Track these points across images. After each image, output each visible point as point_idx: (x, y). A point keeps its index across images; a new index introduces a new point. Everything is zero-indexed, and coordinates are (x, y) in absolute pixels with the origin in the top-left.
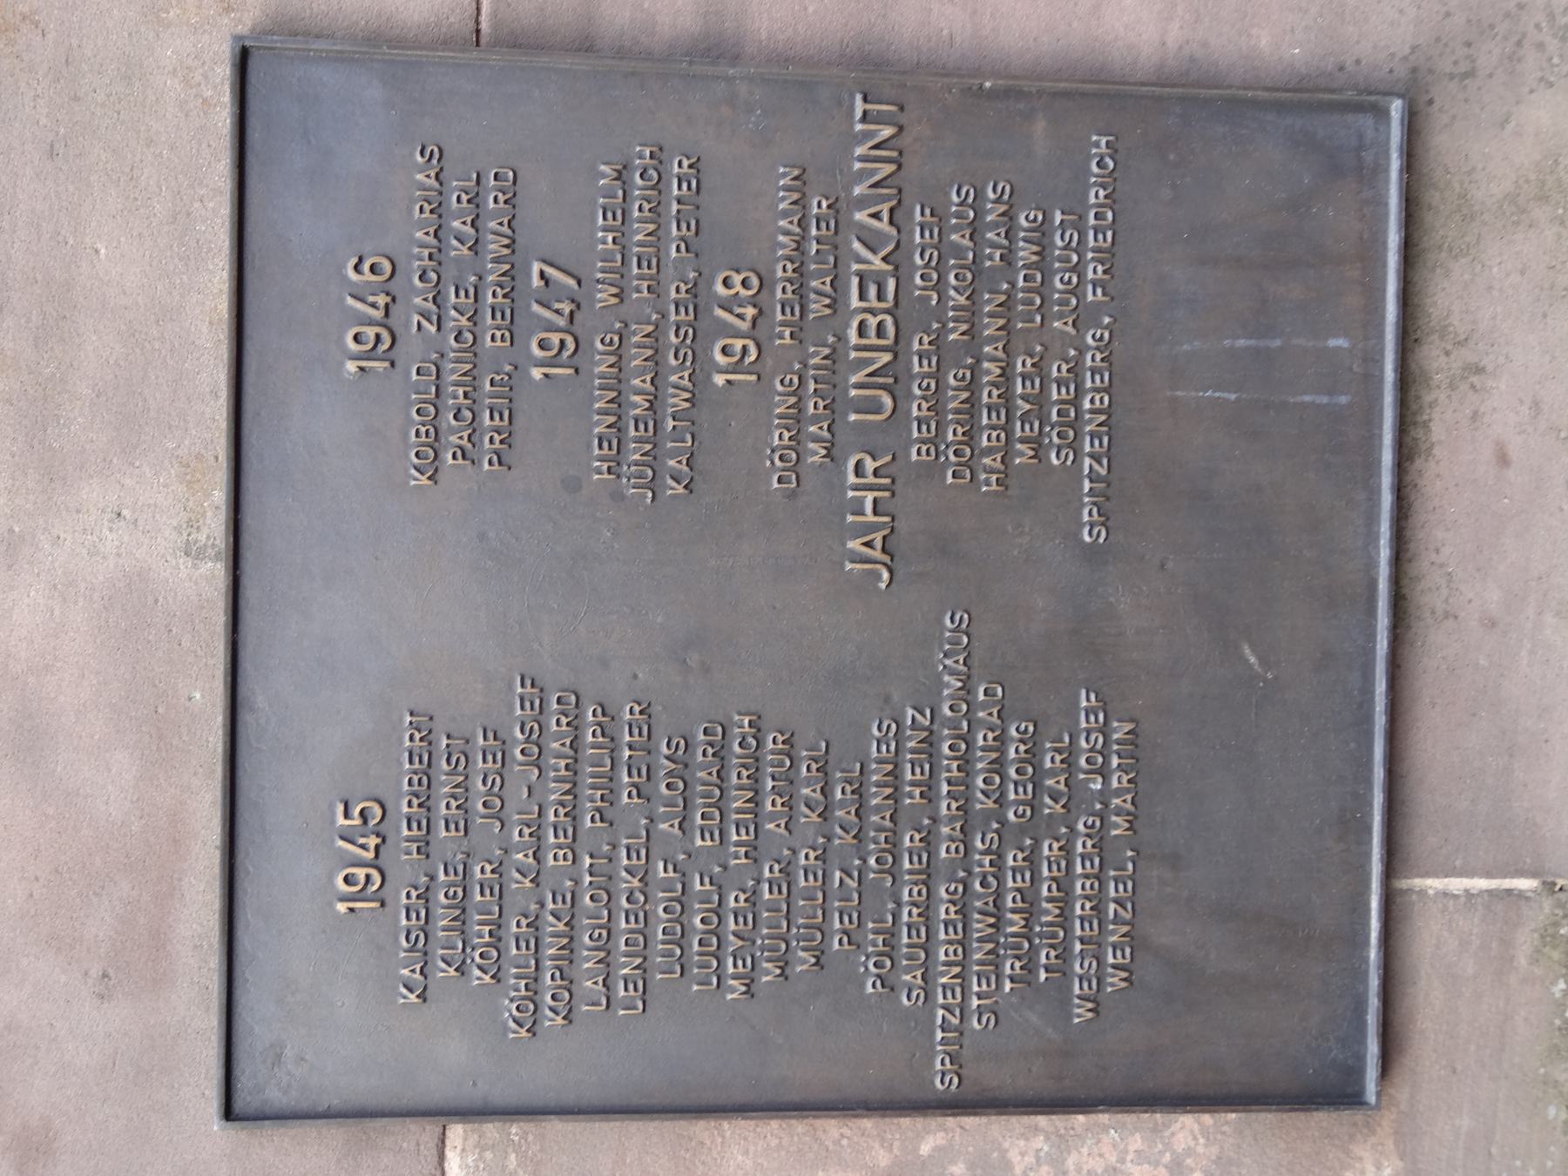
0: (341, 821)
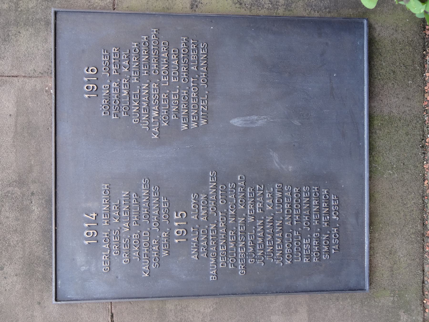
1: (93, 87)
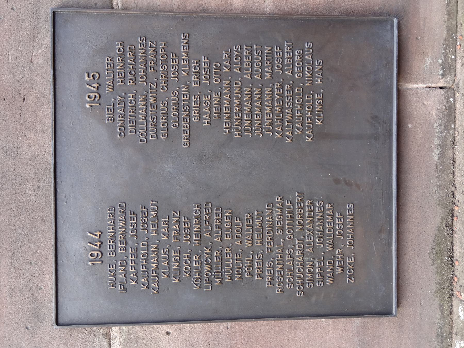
0: (87, 79)
1: (97, 254)
